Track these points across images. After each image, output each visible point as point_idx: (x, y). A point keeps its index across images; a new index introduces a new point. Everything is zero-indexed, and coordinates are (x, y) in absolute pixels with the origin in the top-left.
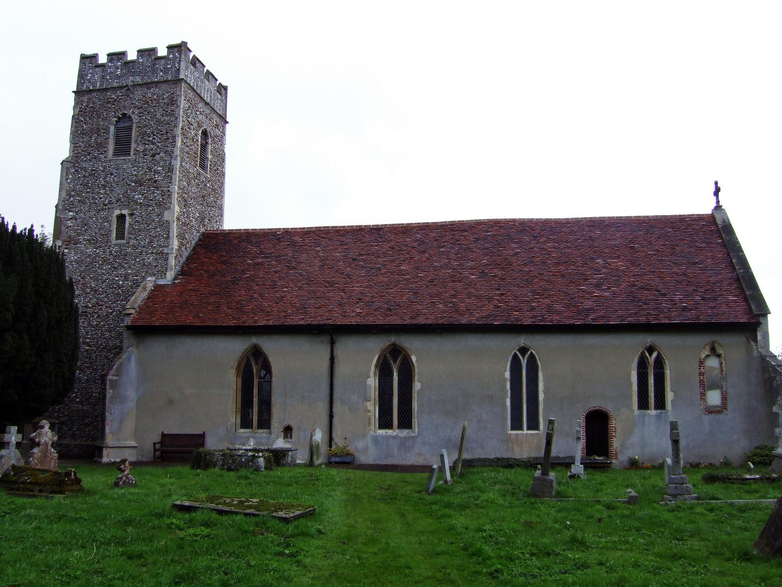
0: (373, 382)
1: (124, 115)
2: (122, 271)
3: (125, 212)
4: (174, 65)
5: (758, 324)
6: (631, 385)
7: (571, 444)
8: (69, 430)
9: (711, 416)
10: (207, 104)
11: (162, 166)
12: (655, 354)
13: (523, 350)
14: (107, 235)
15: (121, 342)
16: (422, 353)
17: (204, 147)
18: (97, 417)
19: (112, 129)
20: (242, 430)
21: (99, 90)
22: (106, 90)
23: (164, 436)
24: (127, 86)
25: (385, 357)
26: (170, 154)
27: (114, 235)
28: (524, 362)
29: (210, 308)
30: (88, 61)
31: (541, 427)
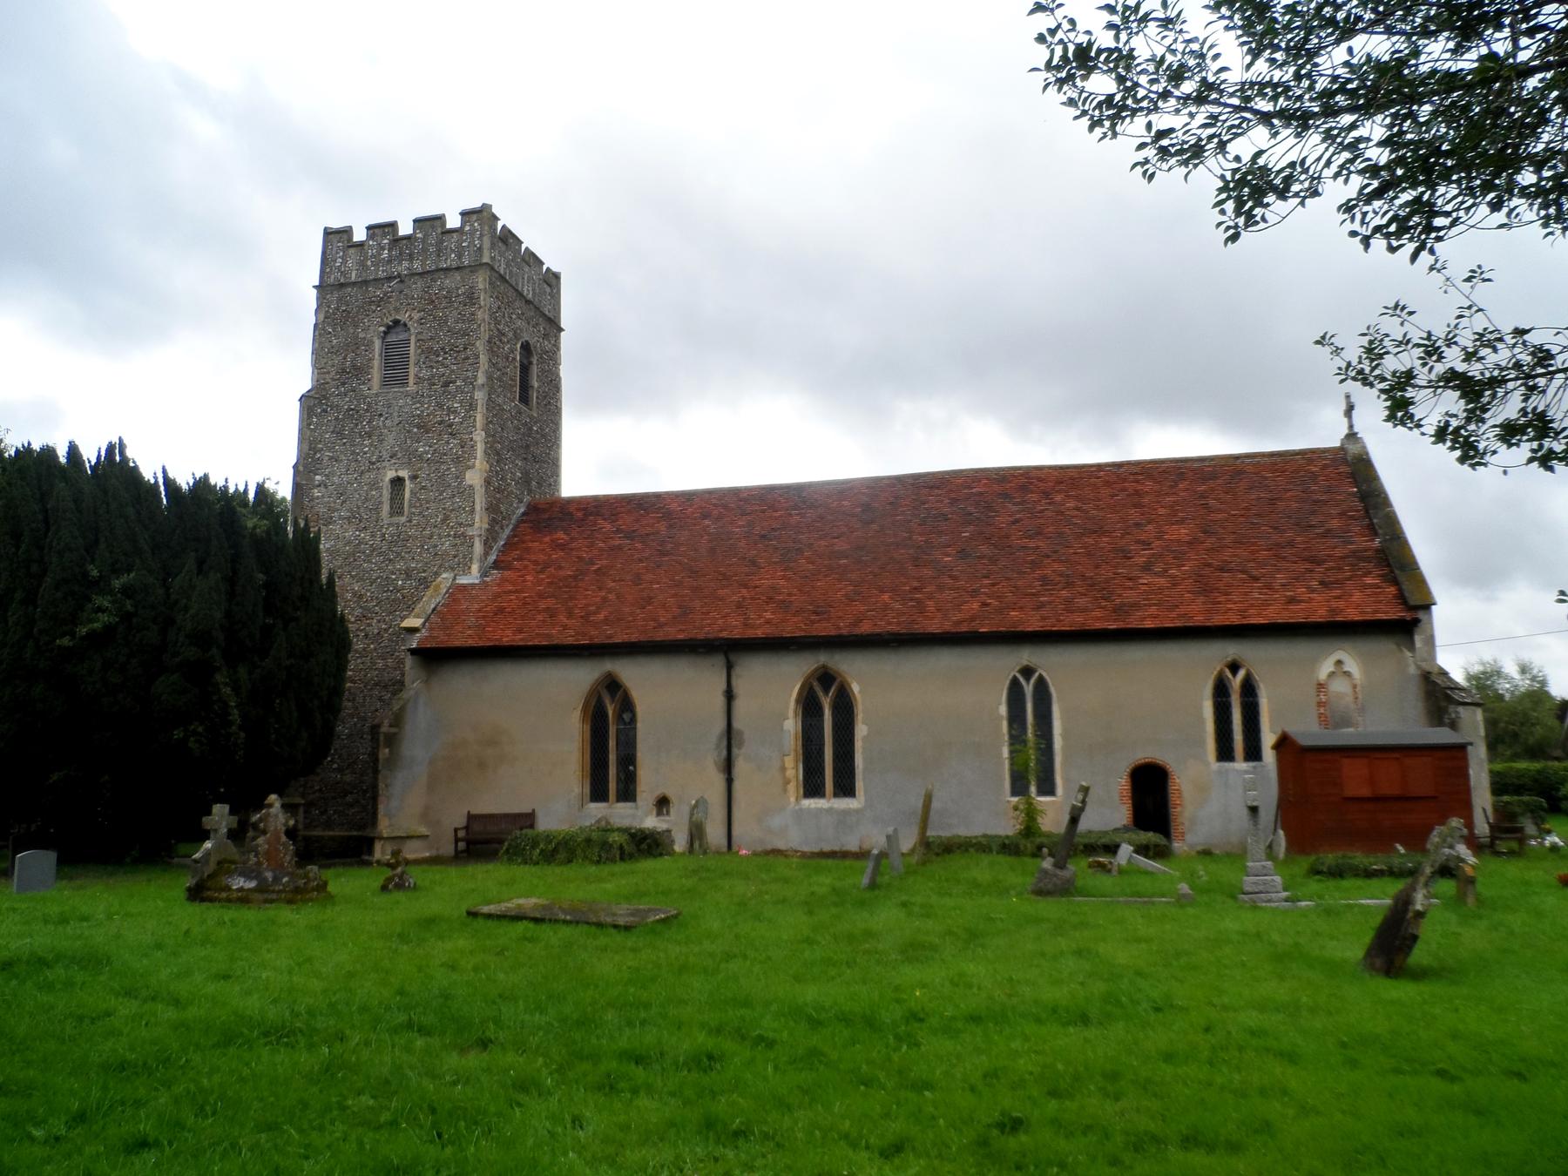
0: (792, 725)
1: (396, 322)
2: (400, 565)
3: (404, 473)
4: (472, 243)
5: (1416, 622)
6: (1202, 721)
7: (1110, 811)
8: (322, 813)
10: (528, 302)
11: (461, 402)
12: (1241, 674)
13: (1027, 672)
14: (377, 509)
15: (403, 675)
16: (866, 678)
17: (525, 369)
18: (365, 792)
19: (377, 344)
20: (593, 805)
21: (354, 284)
22: (366, 283)
23: (471, 818)
24: (399, 275)
25: (811, 689)
26: (470, 382)
27: (386, 508)
28: (1029, 689)
29: (540, 617)
30: (336, 238)
31: (1060, 790)
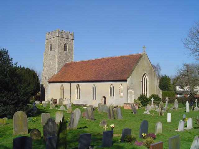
9: (121, 98)
28: (94, 87)
